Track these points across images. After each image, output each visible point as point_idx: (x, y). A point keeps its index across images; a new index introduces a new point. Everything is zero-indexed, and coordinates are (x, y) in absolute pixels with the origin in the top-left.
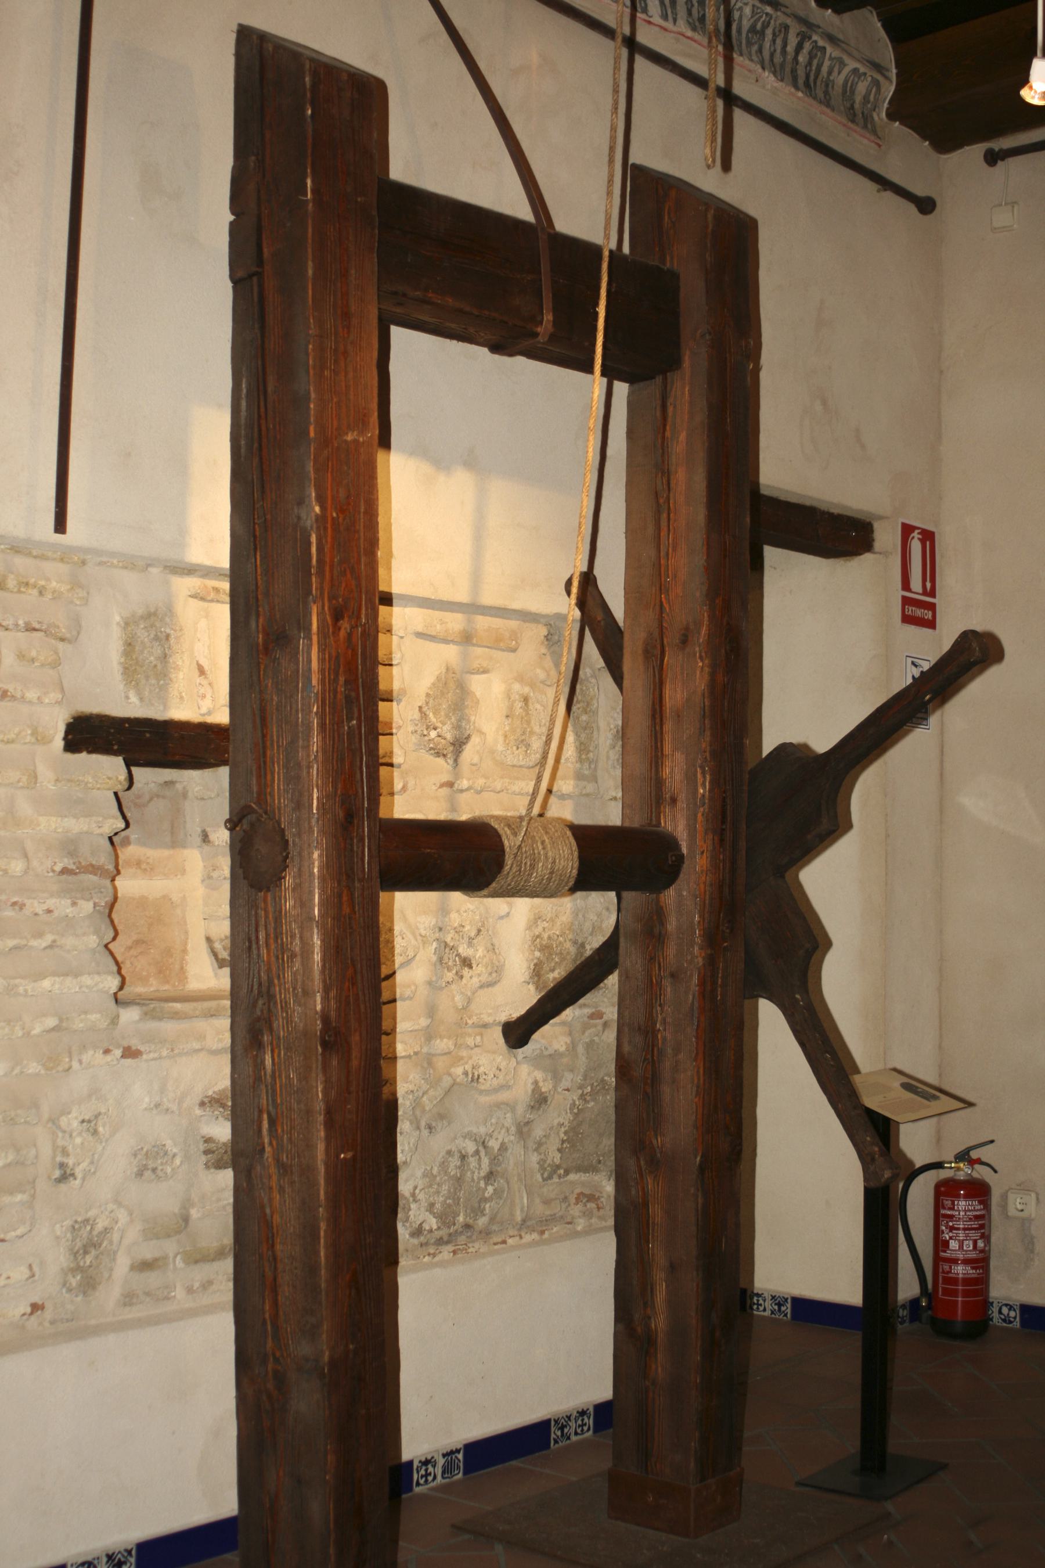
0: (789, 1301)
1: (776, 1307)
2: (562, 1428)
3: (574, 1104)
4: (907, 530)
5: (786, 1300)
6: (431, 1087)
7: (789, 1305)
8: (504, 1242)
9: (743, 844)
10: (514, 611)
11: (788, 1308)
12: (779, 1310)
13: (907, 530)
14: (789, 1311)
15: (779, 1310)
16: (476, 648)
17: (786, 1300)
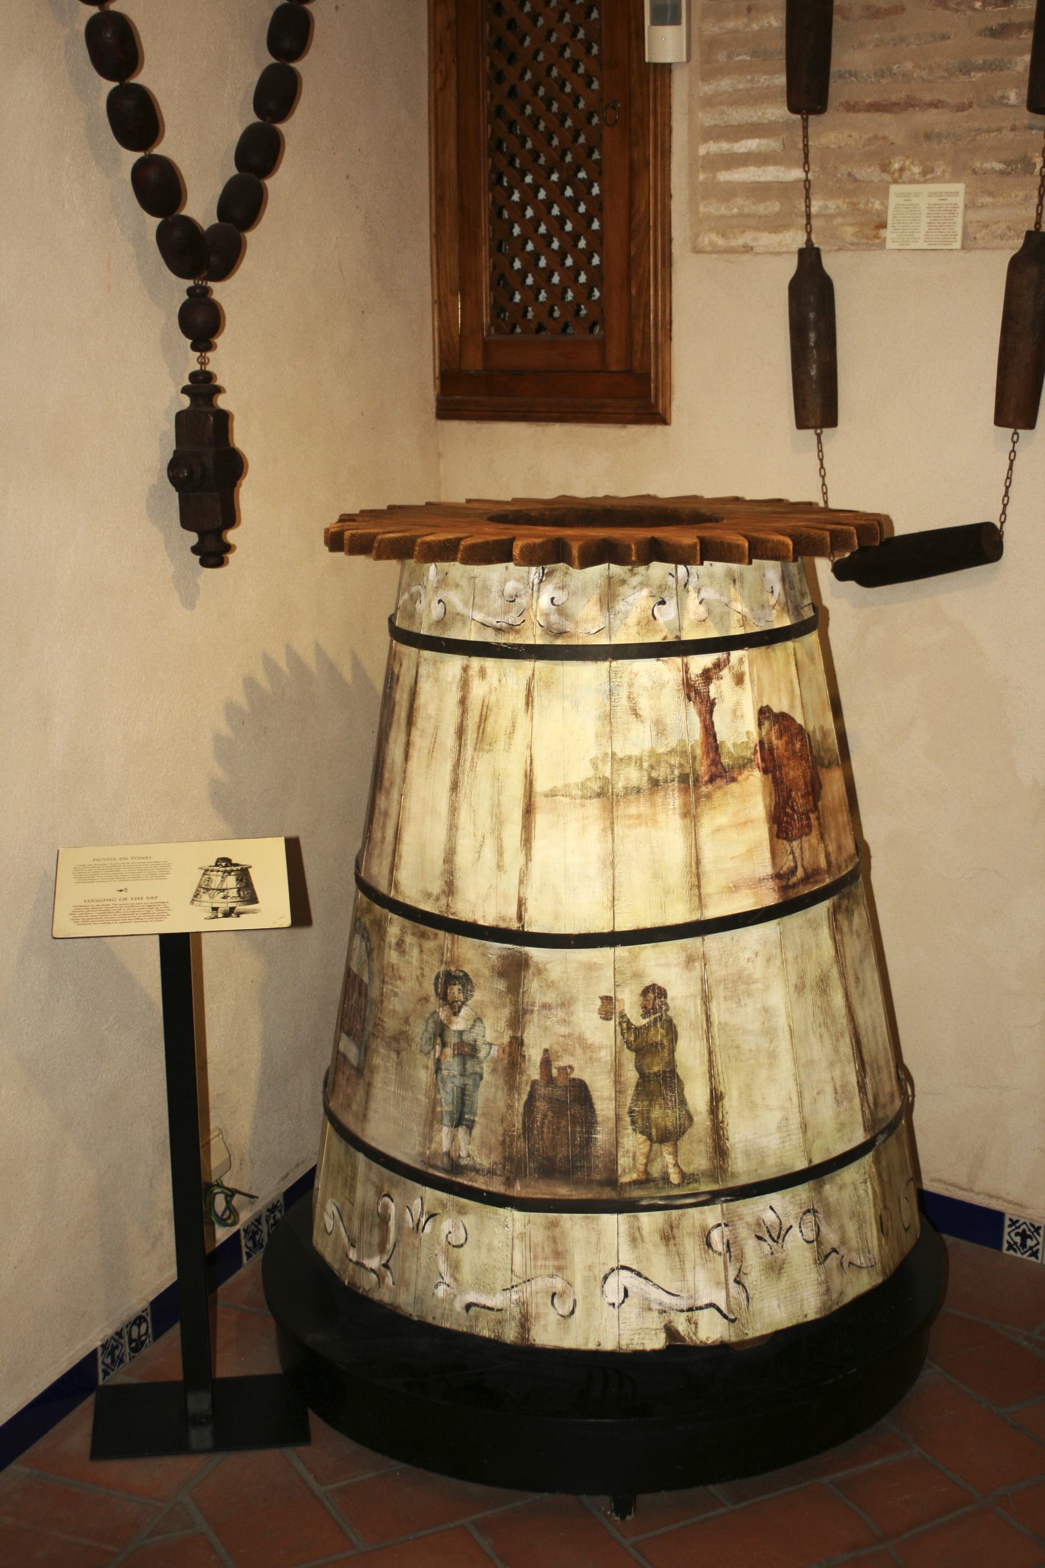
1: (1018, 1239)
2: (112, 1354)
7: (1006, 1237)
15: (1024, 1244)
17: (1037, 1230)
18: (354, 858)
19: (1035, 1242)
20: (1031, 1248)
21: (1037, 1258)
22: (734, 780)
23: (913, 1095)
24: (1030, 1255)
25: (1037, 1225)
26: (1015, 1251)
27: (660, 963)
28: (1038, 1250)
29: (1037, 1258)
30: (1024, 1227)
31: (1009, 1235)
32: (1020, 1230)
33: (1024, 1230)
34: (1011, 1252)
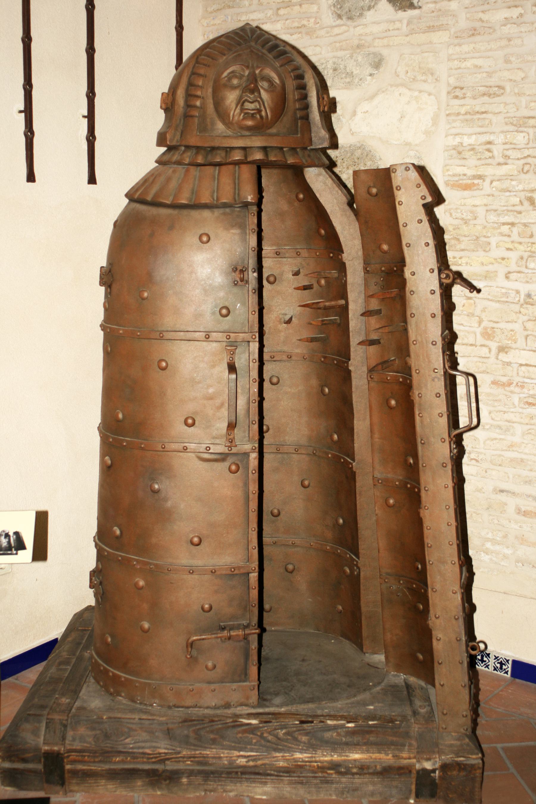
0: (510, 662)
1: (498, 665)
3: (286, 314)
4: (449, 60)
5: (508, 661)
6: (245, 635)
7: (510, 666)
8: (302, 722)
9: (237, 175)
10: (419, 523)
11: (509, 667)
12: (501, 668)
13: (449, 60)
14: (510, 669)
15: (501, 668)
16: (260, 145)
17: (508, 661)
18: (201, 462)
19: (507, 667)
20: (505, 669)
21: (488, 668)
22: (383, 59)
23: (474, 190)
24: (505, 673)
25: (507, 659)
26: (497, 671)
27: (251, 379)
28: (508, 671)
29: (488, 668)
30: (501, 659)
31: (492, 662)
32: (499, 661)
33: (501, 661)
34: (495, 672)
